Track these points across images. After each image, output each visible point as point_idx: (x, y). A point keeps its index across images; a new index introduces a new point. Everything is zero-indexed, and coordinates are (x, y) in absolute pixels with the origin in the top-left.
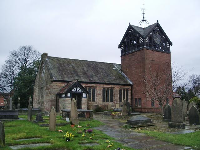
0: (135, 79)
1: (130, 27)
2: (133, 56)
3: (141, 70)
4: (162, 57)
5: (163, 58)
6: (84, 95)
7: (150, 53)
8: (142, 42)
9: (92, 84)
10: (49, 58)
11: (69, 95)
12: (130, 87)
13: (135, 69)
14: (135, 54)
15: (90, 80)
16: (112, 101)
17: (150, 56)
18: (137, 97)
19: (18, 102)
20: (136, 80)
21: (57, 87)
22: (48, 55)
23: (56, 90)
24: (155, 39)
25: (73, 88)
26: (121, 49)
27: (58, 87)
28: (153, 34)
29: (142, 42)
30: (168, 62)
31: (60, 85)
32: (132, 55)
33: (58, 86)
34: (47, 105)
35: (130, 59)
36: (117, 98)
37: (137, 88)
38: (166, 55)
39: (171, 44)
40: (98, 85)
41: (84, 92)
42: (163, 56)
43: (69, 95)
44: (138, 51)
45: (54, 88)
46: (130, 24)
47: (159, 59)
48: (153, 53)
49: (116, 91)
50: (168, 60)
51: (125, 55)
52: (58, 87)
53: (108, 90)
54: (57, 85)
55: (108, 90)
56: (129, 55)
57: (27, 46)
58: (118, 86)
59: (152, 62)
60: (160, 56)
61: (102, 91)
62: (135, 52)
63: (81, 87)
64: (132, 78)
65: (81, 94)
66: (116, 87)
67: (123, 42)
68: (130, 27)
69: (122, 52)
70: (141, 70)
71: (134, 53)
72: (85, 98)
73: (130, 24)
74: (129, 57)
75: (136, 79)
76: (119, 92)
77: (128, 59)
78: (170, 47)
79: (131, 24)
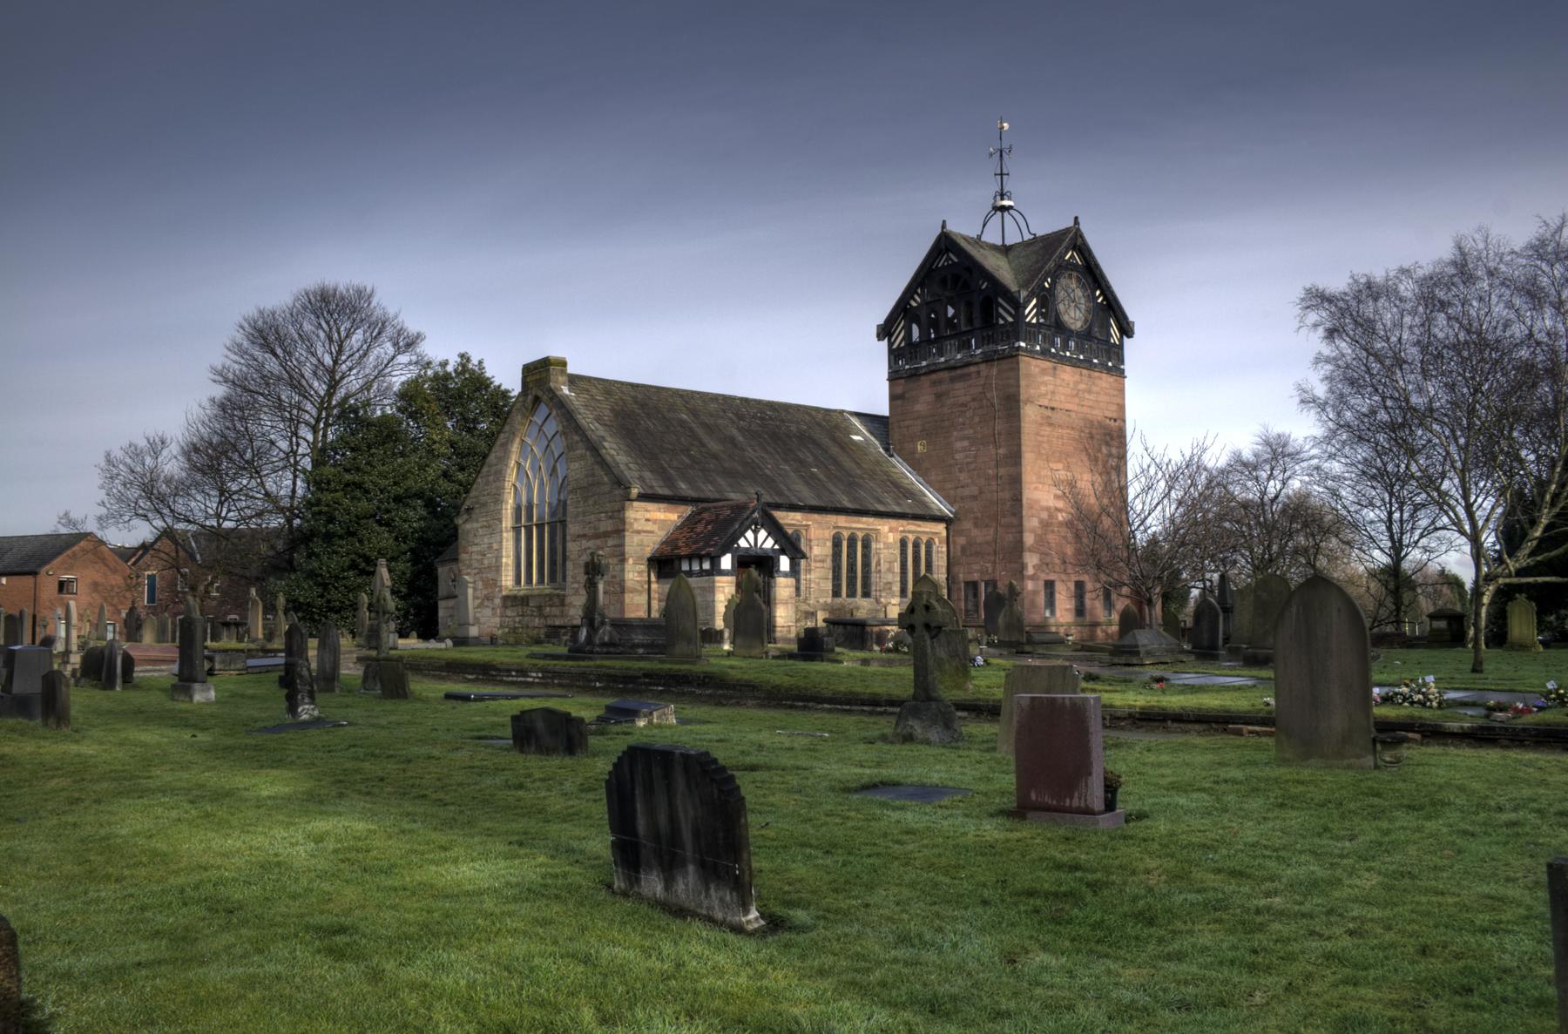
0: (966, 492)
1: (945, 244)
2: (958, 385)
3: (1002, 451)
4: (1090, 392)
5: (1092, 397)
6: (784, 563)
7: (1044, 371)
8: (1010, 319)
9: (792, 515)
10: (574, 380)
11: (726, 562)
12: (941, 528)
13: (966, 443)
14: (969, 375)
15: (780, 493)
16: (866, 594)
17: (1043, 389)
18: (976, 577)
19: (1029, 539)
20: (975, 498)
21: (649, 527)
22: (571, 370)
23: (646, 539)
24: (1061, 307)
25: (742, 534)
26: (890, 344)
27: (655, 528)
28: (1053, 284)
29: (1010, 319)
30: (1115, 415)
31: (661, 516)
32: (953, 380)
33: (655, 522)
34: (976, 567)
35: (939, 396)
36: (890, 577)
37: (975, 532)
38: (1105, 381)
39: (1126, 330)
40: (816, 516)
41: (783, 551)
42: (1095, 389)
43: (726, 562)
44: (988, 359)
45: (639, 532)
46: (944, 226)
47: (1077, 400)
48: (1054, 375)
49: (887, 546)
50: (1114, 408)
51: (914, 375)
52: (655, 528)
53: (852, 541)
54: (648, 516)
55: (852, 541)
56: (934, 376)
57: (290, 302)
58: (893, 523)
59: (1049, 413)
60: (1082, 386)
61: (829, 544)
62: (968, 365)
63: (776, 530)
64: (948, 486)
65: (771, 558)
66: (886, 528)
67: (902, 311)
68: (945, 244)
69: (894, 355)
70: (1002, 451)
71: (966, 370)
72: (786, 575)
73: (944, 226)
74: (934, 383)
75: (974, 490)
76: (897, 552)
77: (930, 398)
78: (1121, 347)
79: (950, 227)
